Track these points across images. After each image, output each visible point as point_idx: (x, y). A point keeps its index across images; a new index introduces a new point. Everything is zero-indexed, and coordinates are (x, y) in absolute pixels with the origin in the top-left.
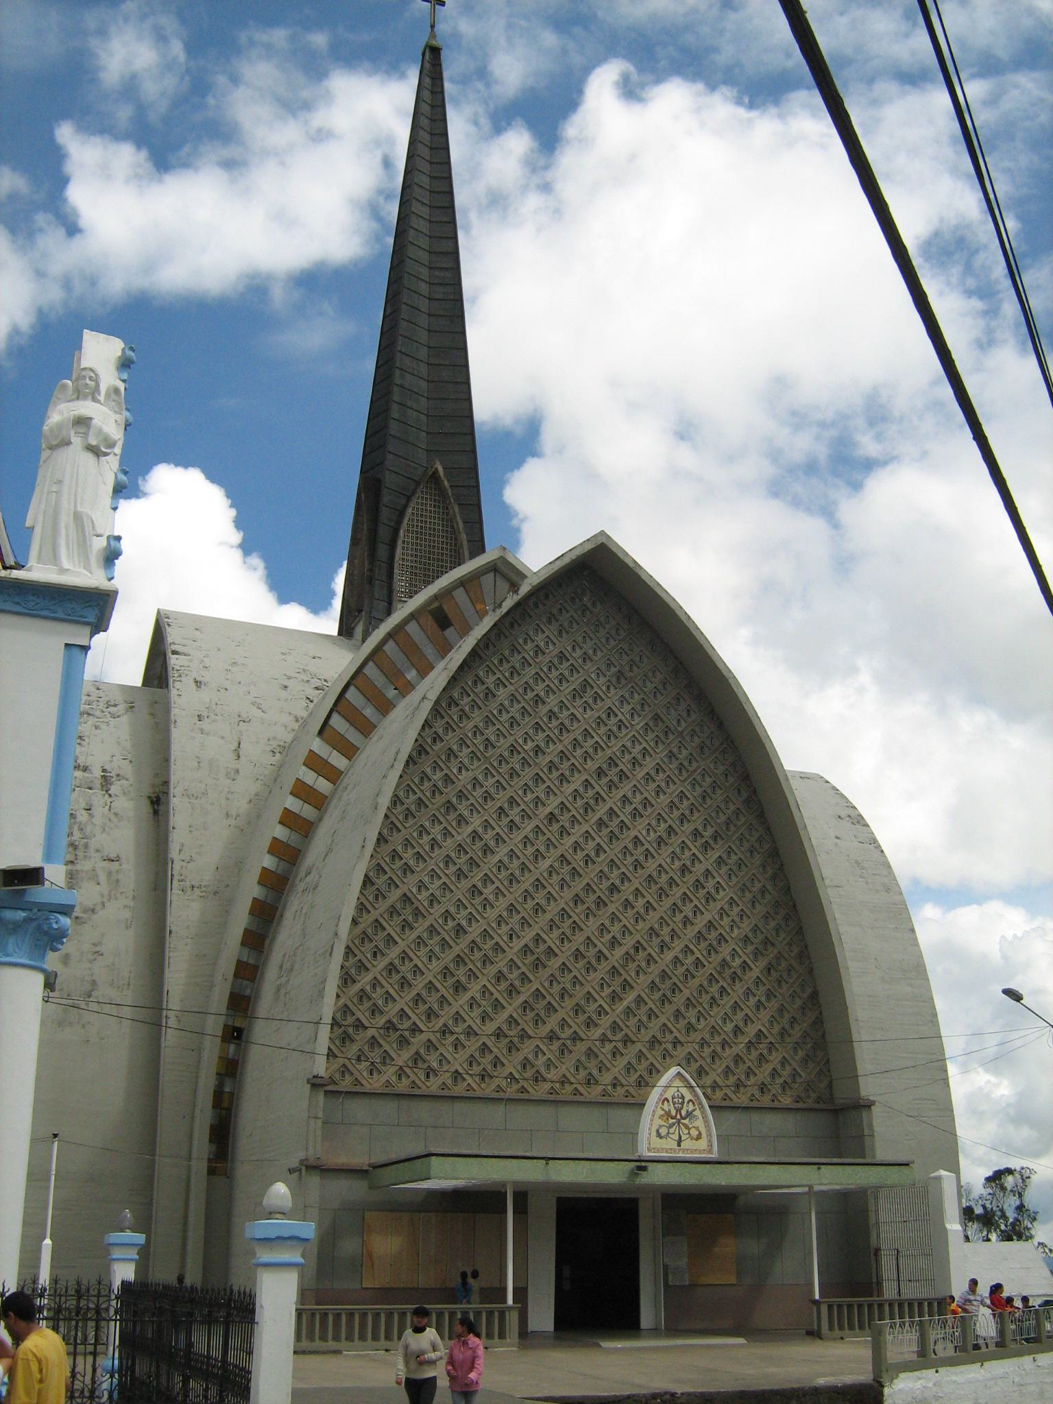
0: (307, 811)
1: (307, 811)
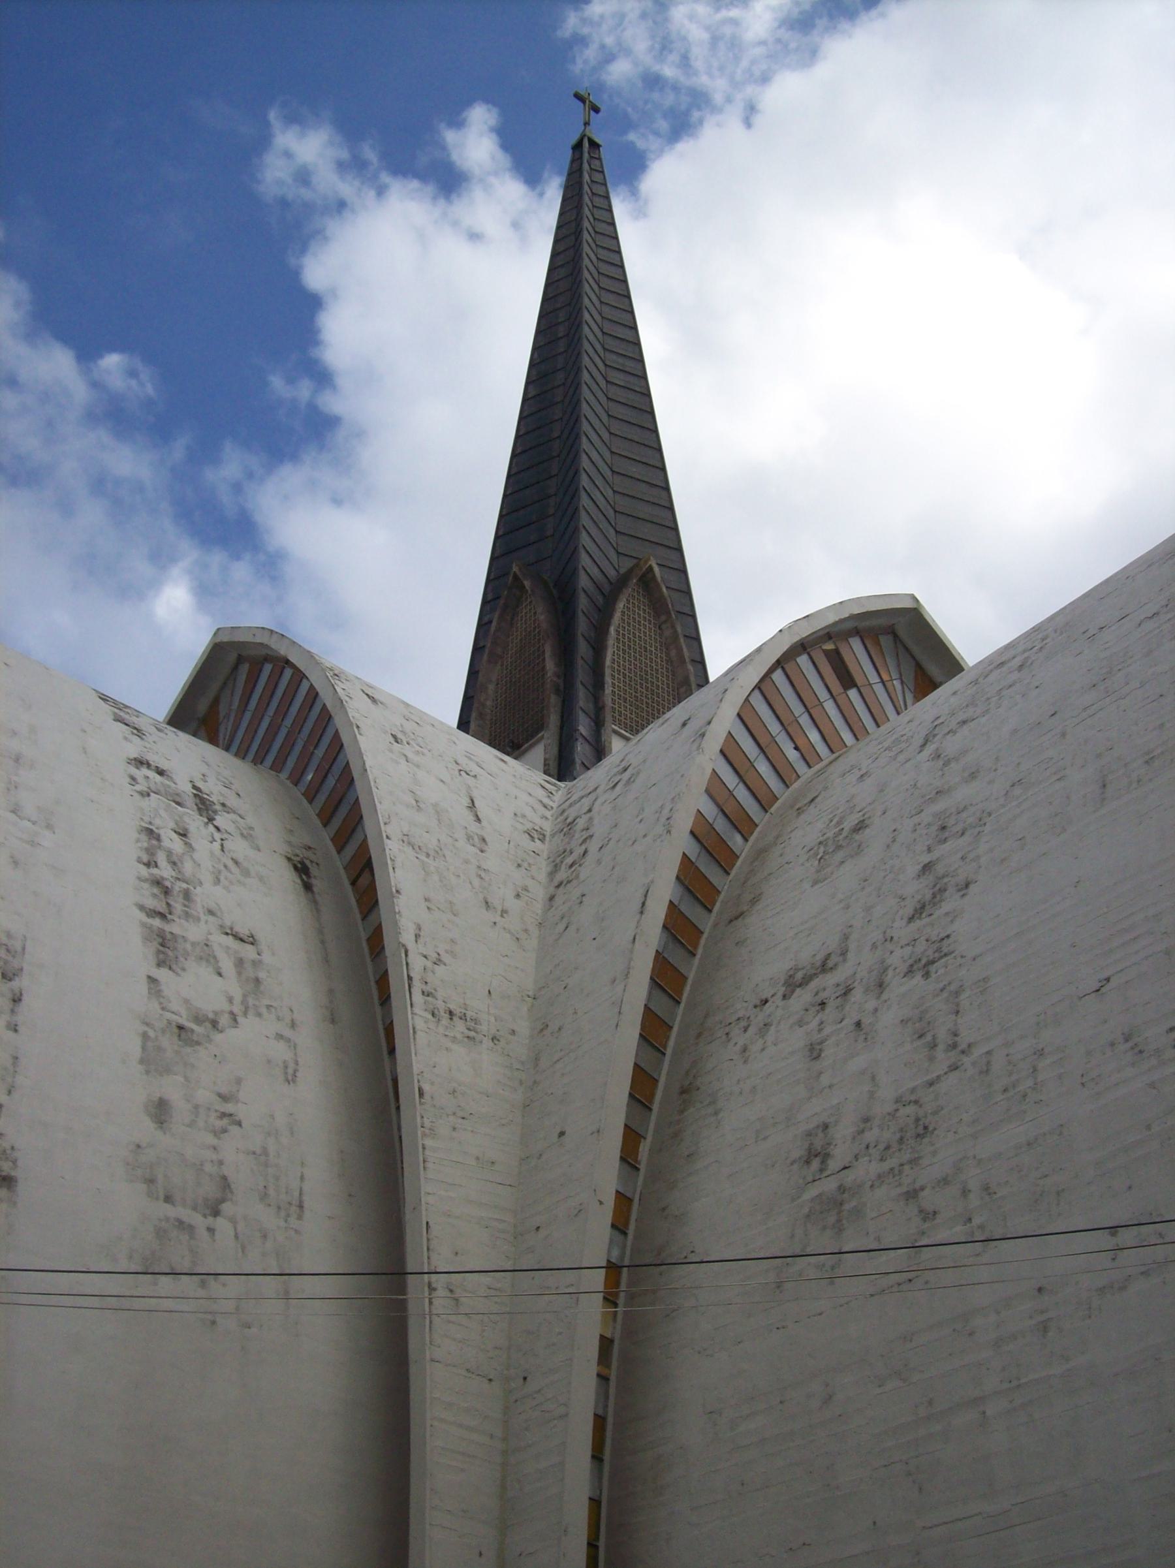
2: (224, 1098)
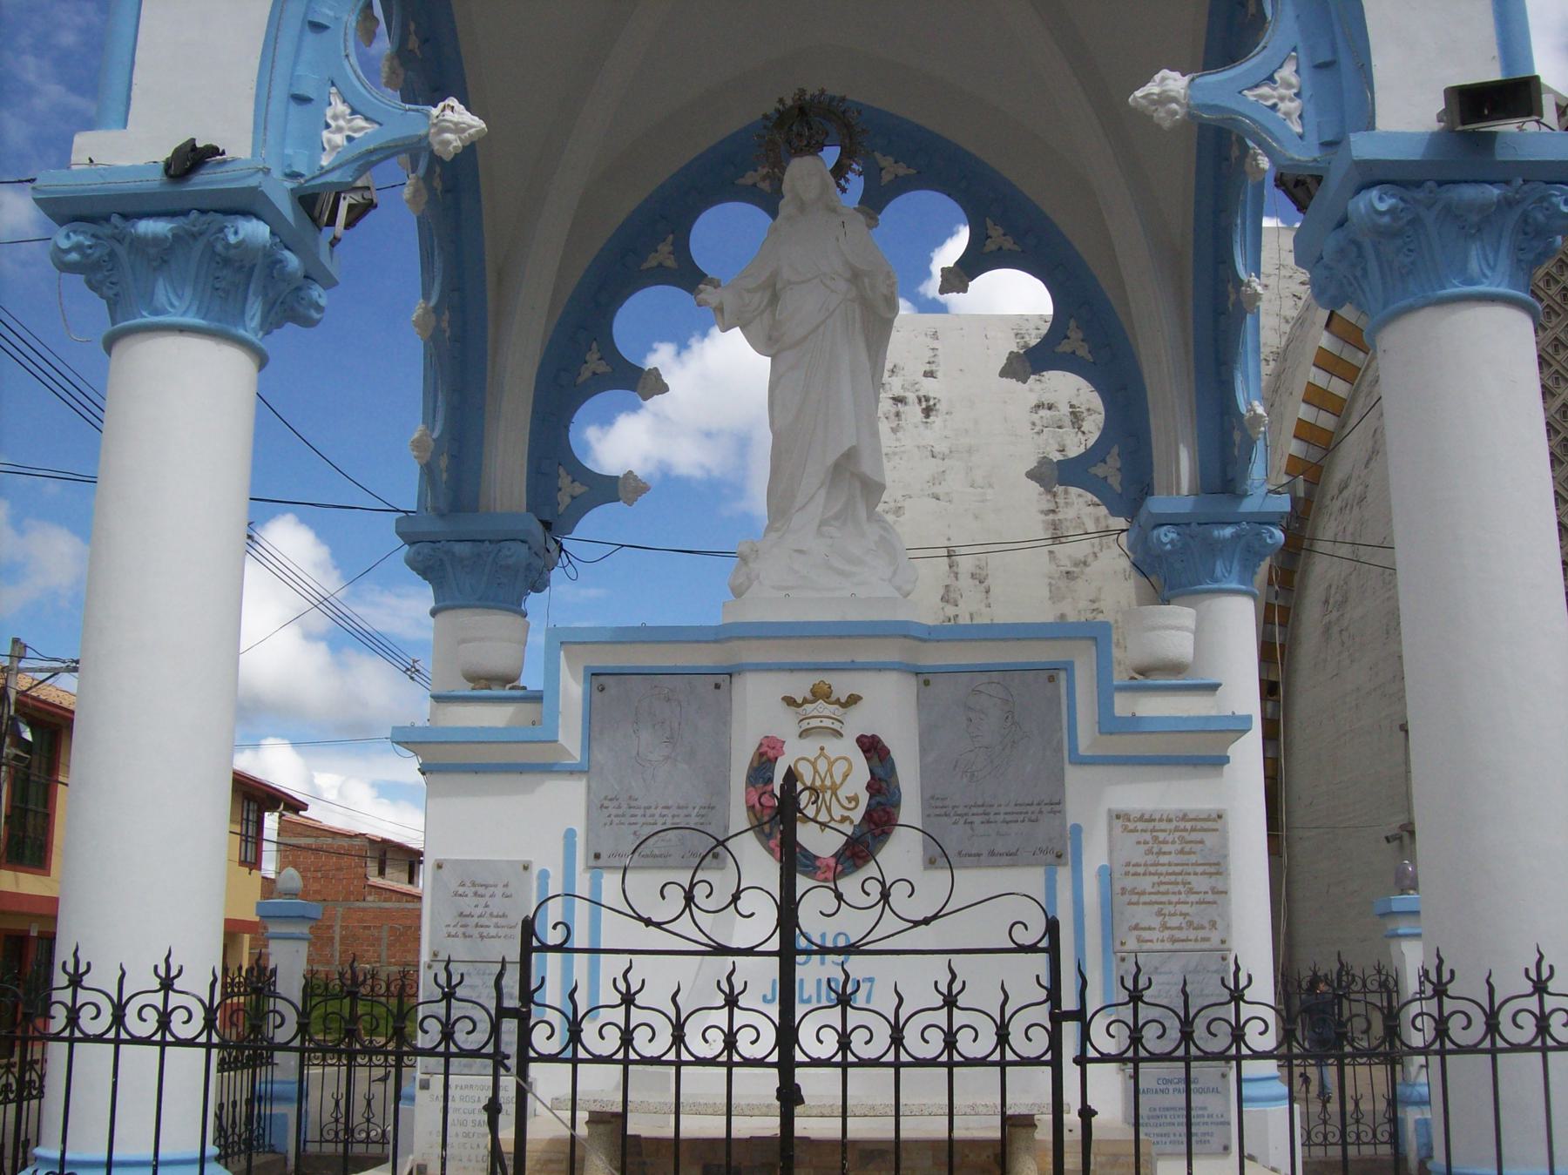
0: (1326, 420)
1: (1326, 420)
2: (1093, 601)
